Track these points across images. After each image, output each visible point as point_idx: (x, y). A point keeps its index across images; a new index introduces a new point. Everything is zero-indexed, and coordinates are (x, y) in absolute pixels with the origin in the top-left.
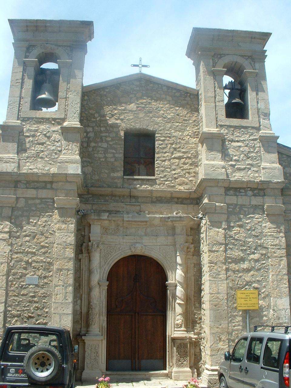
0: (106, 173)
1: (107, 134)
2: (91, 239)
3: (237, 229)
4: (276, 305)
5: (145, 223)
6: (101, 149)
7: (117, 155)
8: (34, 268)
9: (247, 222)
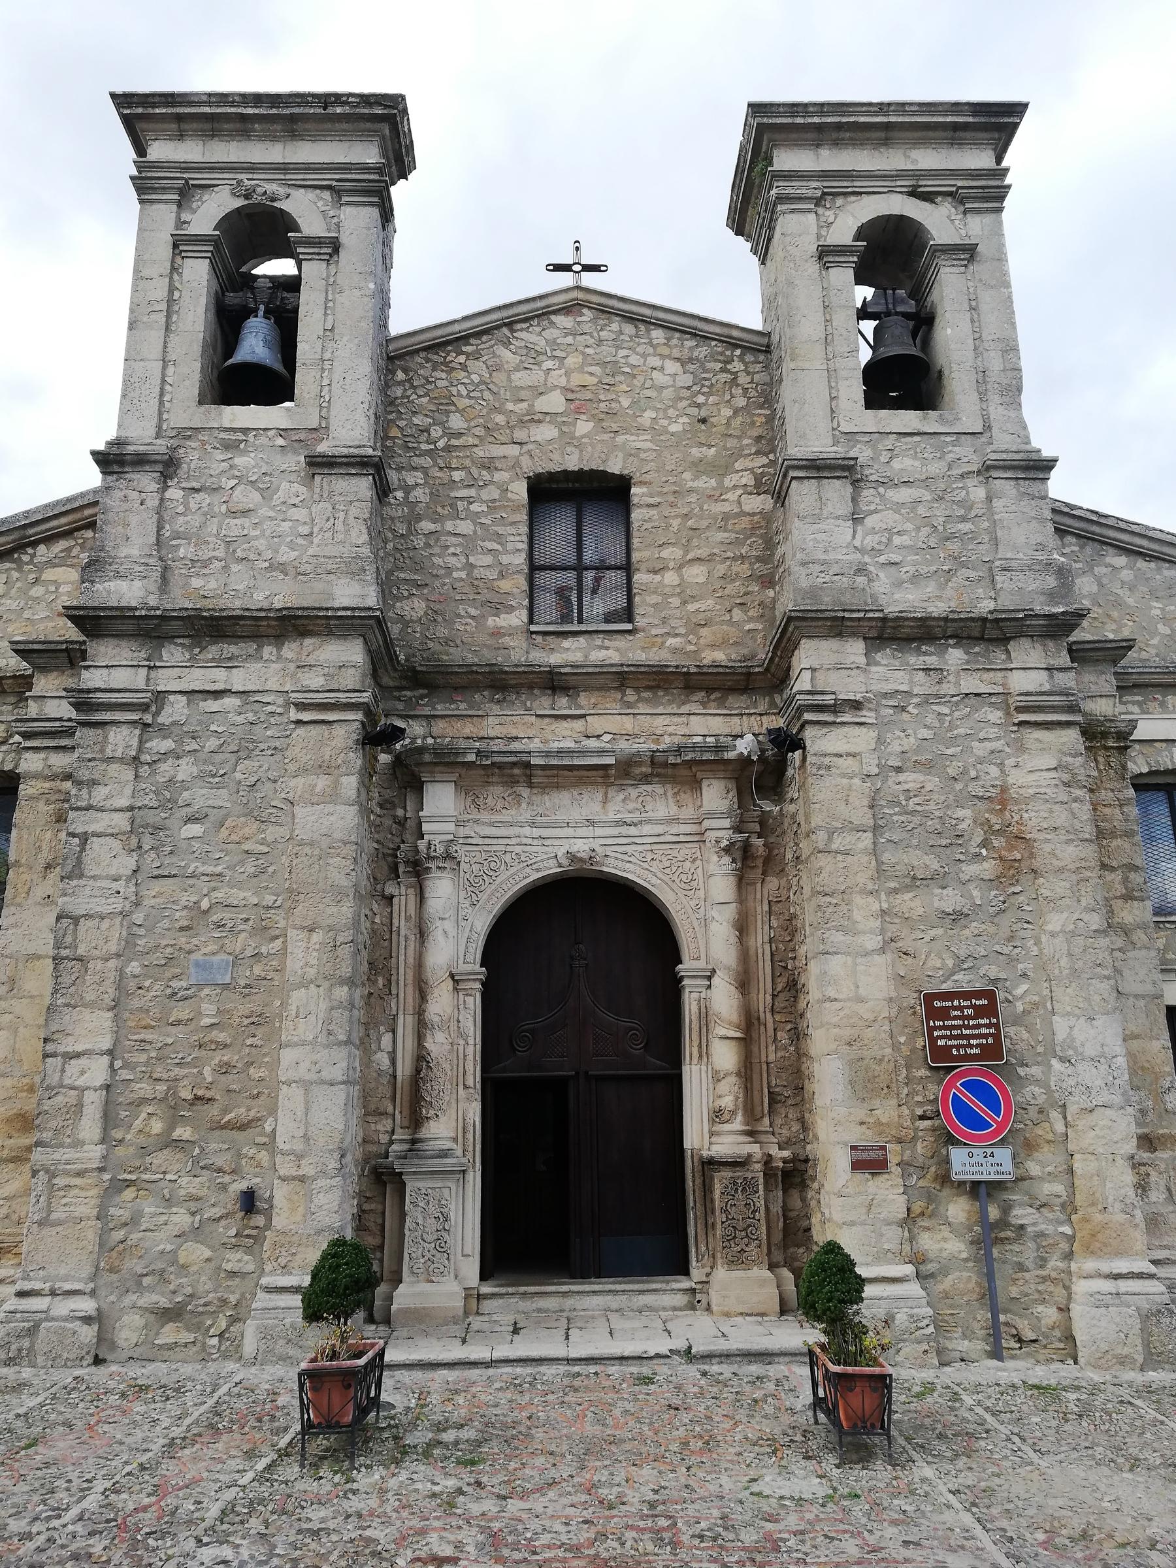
0: (472, 617)
1: (472, 492)
2: (425, 827)
3: (914, 776)
4: (1073, 1040)
5: (601, 773)
6: (453, 539)
7: (505, 559)
8: (219, 925)
9: (949, 752)
